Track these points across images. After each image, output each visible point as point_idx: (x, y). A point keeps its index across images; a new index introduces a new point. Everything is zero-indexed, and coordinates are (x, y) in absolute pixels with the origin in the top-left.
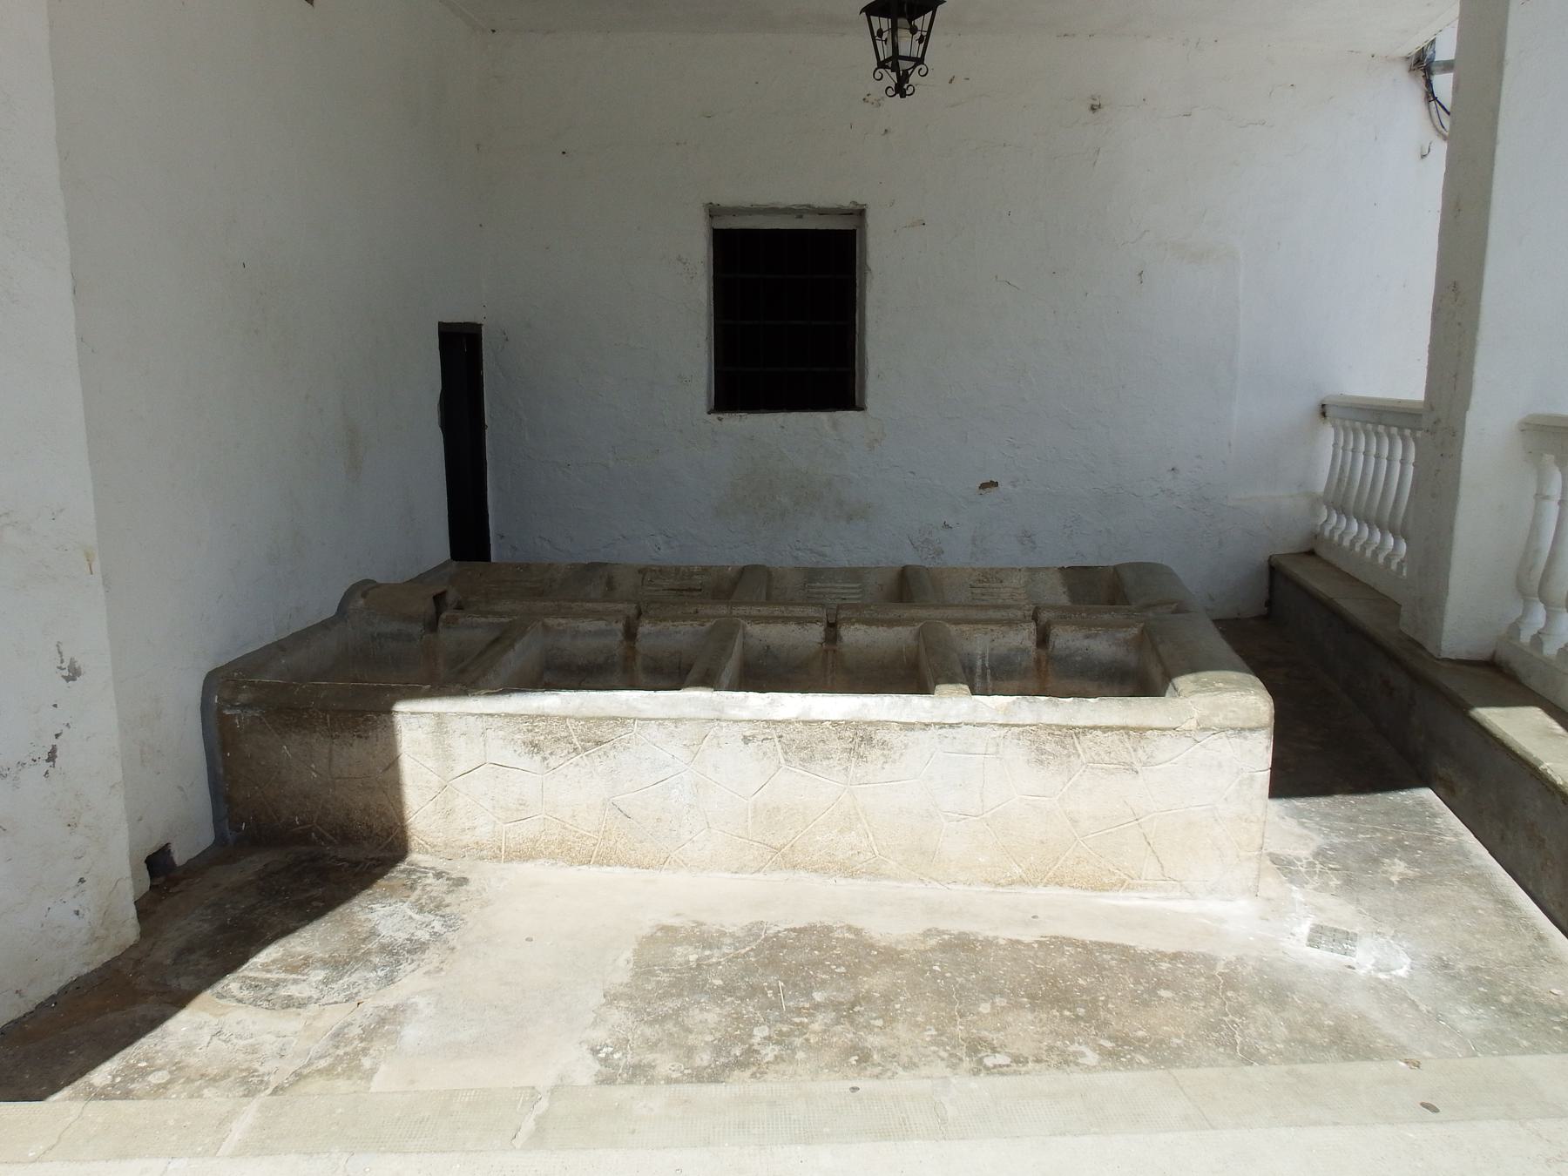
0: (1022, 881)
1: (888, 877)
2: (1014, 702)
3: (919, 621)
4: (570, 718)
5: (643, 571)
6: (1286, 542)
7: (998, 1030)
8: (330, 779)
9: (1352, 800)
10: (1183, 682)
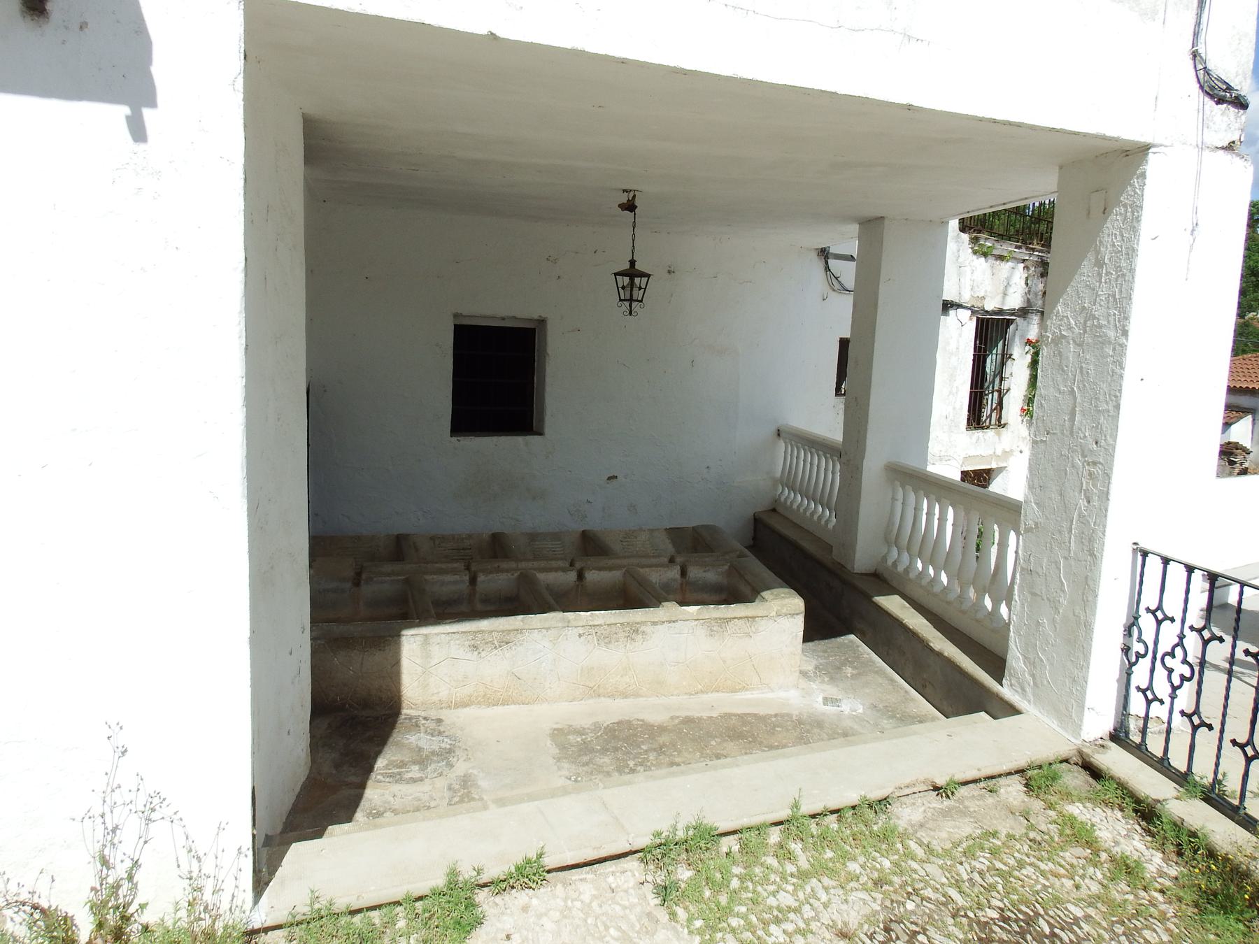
0: (702, 692)
1: (642, 696)
2: (927, 626)
3: (624, 567)
4: (494, 631)
5: (433, 538)
6: (761, 505)
7: (723, 750)
8: (360, 674)
9: (823, 642)
10: (765, 594)
